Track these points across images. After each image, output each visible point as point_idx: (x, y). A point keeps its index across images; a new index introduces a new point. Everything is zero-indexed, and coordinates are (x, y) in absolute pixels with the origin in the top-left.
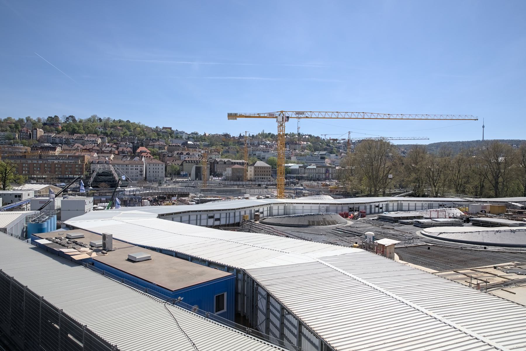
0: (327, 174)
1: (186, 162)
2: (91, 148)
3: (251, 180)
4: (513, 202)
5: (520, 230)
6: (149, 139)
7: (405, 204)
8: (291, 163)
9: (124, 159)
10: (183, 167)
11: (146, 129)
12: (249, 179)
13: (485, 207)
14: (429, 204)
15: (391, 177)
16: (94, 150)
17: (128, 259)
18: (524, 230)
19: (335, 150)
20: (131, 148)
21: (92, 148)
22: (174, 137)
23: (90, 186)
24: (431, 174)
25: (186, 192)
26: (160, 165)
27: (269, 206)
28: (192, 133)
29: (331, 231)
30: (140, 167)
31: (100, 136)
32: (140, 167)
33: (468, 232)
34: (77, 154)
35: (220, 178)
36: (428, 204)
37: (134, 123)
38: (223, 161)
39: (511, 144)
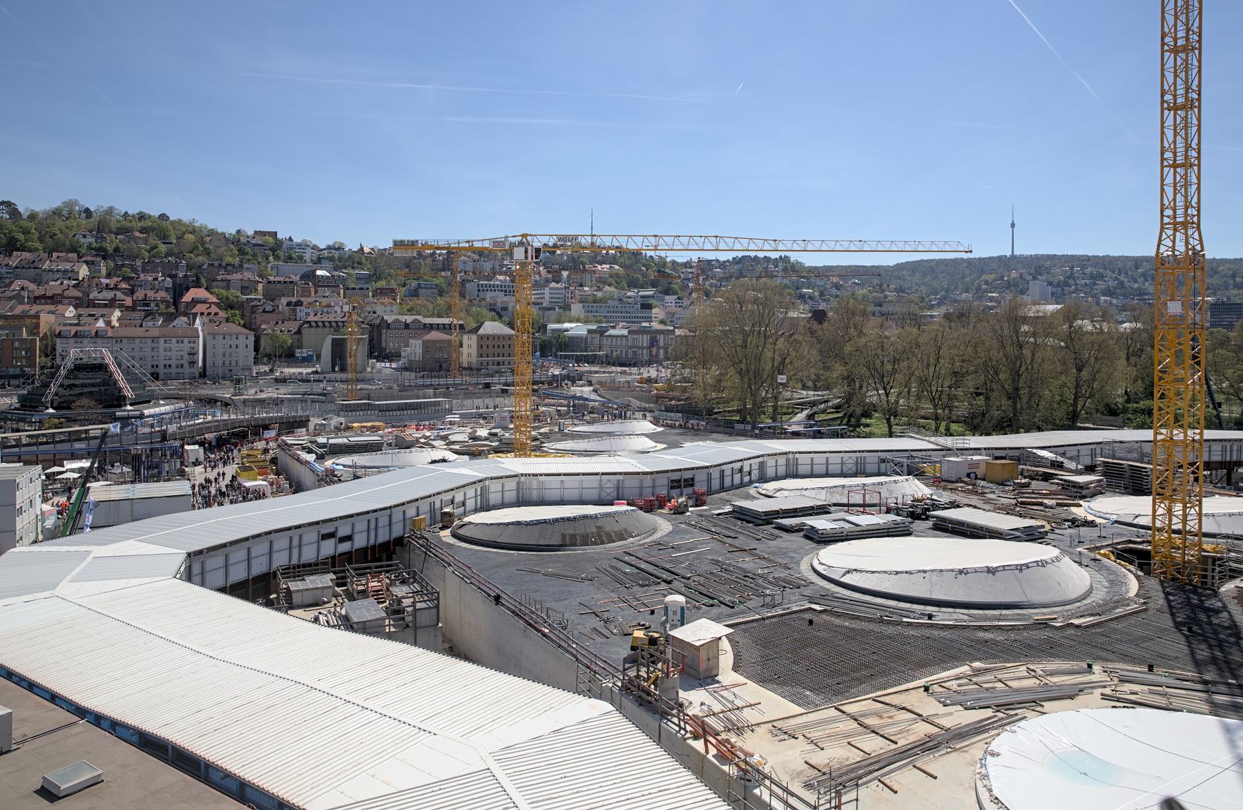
0: (654, 350)
1: (310, 326)
2: (59, 295)
3: (470, 369)
4: (1037, 448)
5: (1006, 568)
6: (216, 264)
7: (803, 459)
8: (571, 321)
9: (148, 323)
10: (302, 338)
11: (209, 238)
12: (465, 365)
13: (976, 464)
14: (857, 458)
15: (785, 381)
16: (66, 298)
17: (42, 786)
18: (1013, 567)
19: (677, 283)
20: (167, 289)
21: (61, 292)
22: (283, 258)
23: (49, 405)
24: (878, 362)
25: (301, 417)
26: (242, 338)
27: (479, 486)
28: (329, 248)
29: (612, 567)
30: (190, 342)
31: (84, 259)
32: (190, 342)
33: (902, 572)
34: (18, 311)
35: (394, 365)
36: (855, 459)
37: (179, 222)
38: (401, 322)
39: (1070, 265)
